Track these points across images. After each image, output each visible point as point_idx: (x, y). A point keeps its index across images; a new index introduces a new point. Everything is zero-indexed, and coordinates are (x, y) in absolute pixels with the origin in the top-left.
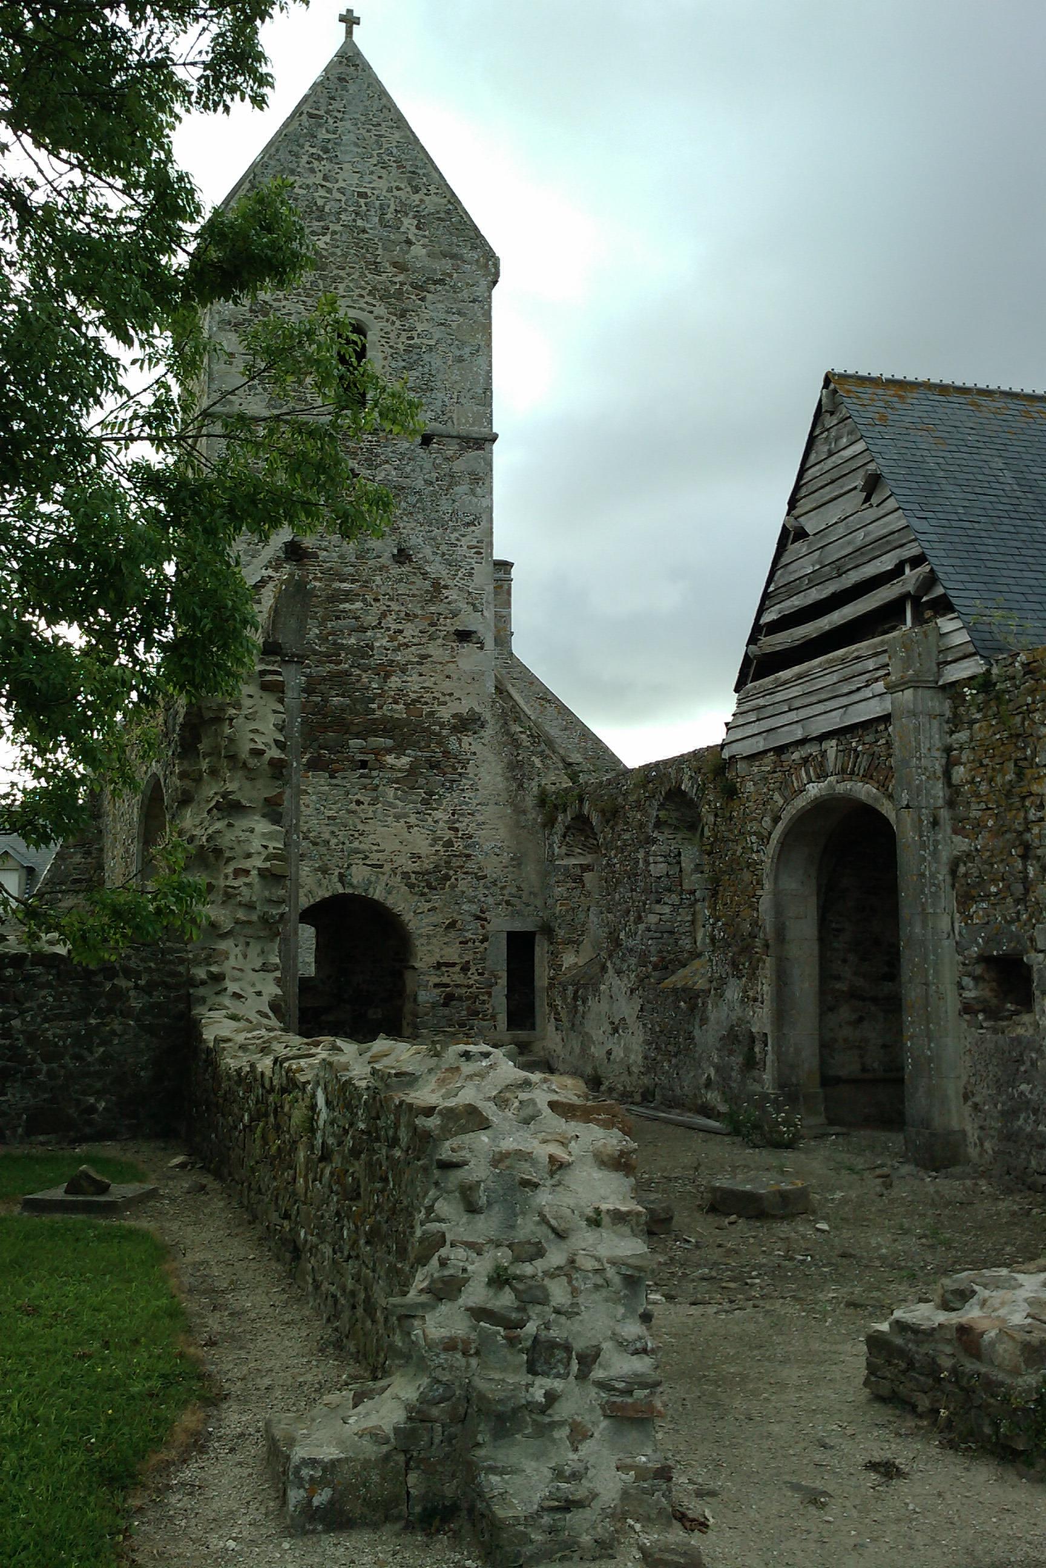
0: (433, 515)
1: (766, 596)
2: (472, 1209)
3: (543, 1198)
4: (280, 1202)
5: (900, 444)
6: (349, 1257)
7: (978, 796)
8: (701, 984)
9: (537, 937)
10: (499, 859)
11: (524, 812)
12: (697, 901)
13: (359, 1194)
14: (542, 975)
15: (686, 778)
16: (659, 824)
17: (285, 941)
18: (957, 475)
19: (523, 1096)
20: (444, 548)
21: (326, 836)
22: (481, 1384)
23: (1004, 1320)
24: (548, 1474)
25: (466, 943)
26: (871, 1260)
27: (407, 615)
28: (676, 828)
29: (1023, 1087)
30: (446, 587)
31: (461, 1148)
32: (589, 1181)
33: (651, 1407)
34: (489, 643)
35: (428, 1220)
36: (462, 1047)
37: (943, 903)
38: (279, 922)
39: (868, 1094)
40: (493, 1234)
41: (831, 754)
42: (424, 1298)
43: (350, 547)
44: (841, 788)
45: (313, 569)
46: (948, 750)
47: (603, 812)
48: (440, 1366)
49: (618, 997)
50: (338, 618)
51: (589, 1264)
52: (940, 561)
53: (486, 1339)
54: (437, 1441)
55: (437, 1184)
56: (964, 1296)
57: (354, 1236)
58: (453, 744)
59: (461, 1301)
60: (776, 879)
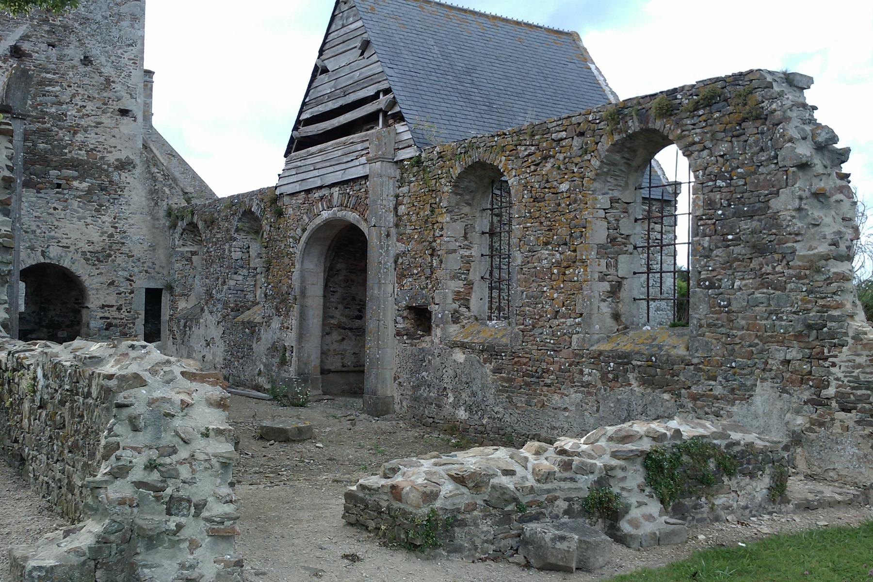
0: (107, 38)
1: (304, 104)
2: (135, 429)
3: (177, 422)
4: (12, 433)
5: (381, 25)
6: (58, 460)
7: (411, 222)
8: (258, 319)
9: (164, 292)
10: (142, 246)
11: (158, 219)
12: (257, 274)
13: (64, 425)
14: (166, 313)
15: (254, 204)
16: (237, 230)
17: (11, 287)
18: (411, 46)
19: (166, 369)
20: (113, 58)
21: (34, 228)
22: (139, 521)
23: (413, 482)
24: (177, 567)
25: (120, 294)
26: (344, 461)
27: (89, 97)
28: (248, 233)
29: (424, 373)
30: (114, 82)
31: (129, 397)
32: (202, 412)
33: (233, 529)
34: (140, 118)
35: (109, 435)
36: (130, 342)
37: (390, 278)
38: (8, 275)
39: (347, 379)
40: (147, 443)
41: (336, 195)
42: (106, 478)
43: (53, 53)
44: (340, 214)
45: (29, 64)
46: (397, 196)
47: (205, 221)
48: (116, 513)
49: (210, 326)
50: (44, 95)
51: (202, 457)
52: (398, 92)
53: (142, 498)
54: (113, 553)
55: (115, 416)
56: (395, 470)
57: (61, 449)
58: (115, 177)
59: (128, 479)
60: (302, 262)
